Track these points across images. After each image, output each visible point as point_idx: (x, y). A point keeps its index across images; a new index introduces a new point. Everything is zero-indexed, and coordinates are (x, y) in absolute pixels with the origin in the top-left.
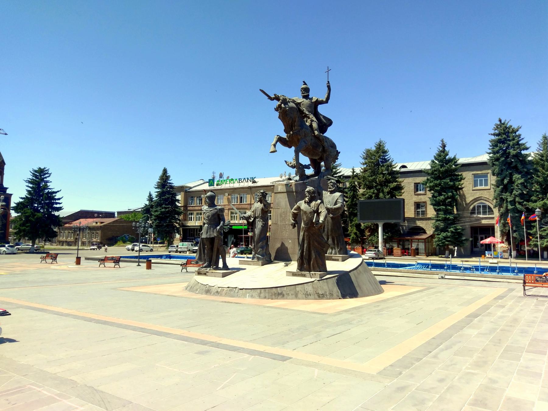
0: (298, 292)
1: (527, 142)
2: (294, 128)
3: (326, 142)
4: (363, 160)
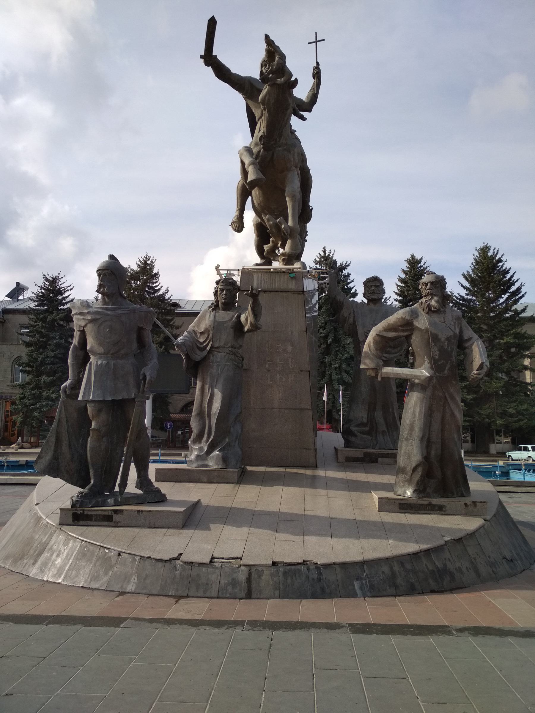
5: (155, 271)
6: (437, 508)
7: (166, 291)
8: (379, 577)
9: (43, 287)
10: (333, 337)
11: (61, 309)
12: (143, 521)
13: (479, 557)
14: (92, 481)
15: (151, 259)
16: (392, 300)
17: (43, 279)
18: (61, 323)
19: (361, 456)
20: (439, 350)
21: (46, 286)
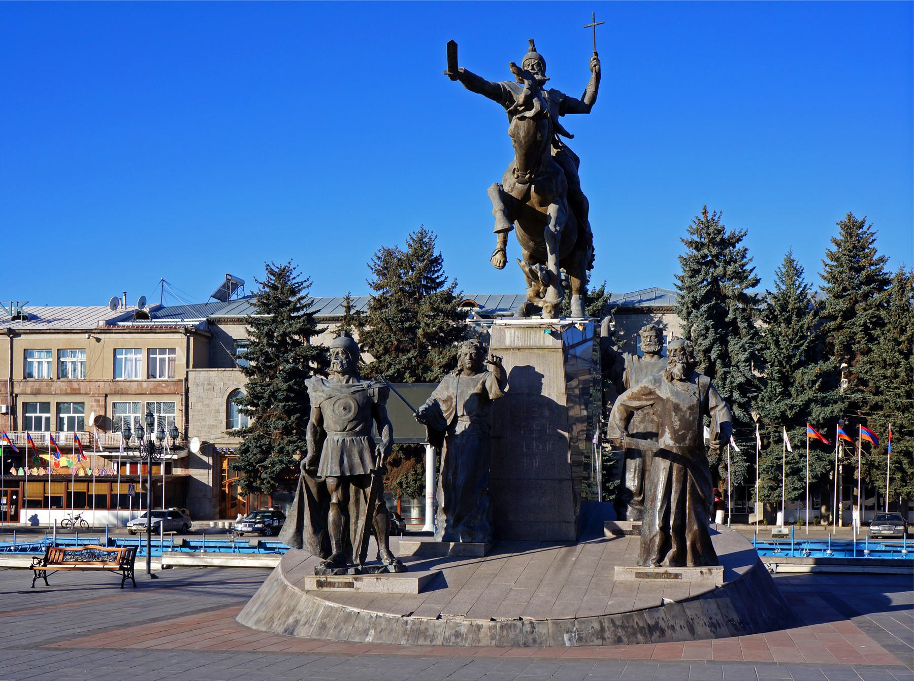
0: (692, 619)
1: (754, 268)
5: (436, 254)
6: (672, 576)
7: (454, 285)
9: (267, 283)
10: (720, 350)
11: (295, 317)
12: (382, 587)
15: (429, 235)
16: (815, 288)
17: (267, 272)
18: (296, 337)
19: (629, 529)
20: (680, 420)
21: (271, 281)
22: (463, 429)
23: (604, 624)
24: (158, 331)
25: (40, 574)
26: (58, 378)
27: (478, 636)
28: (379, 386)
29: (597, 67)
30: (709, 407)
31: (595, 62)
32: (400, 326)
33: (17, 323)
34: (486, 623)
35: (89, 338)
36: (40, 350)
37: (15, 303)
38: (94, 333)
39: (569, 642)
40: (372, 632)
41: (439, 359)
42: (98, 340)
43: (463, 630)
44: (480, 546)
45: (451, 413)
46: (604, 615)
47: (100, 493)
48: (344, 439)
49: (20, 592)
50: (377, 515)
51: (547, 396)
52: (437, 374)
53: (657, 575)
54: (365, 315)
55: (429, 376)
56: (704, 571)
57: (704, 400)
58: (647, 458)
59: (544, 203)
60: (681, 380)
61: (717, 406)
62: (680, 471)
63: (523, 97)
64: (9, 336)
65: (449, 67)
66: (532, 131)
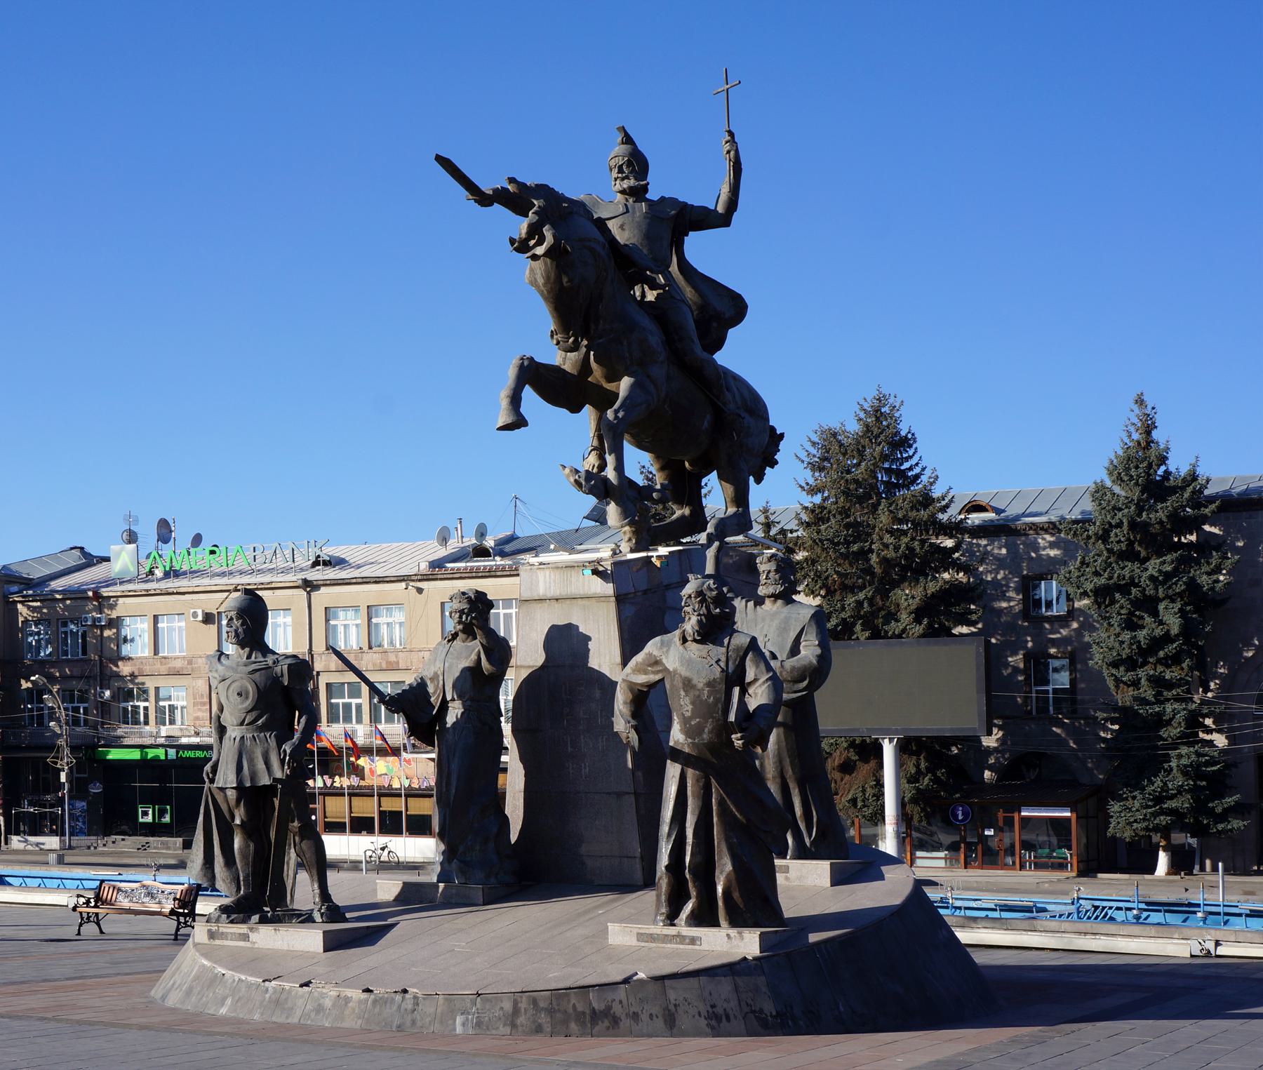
0: (675, 1005)
2: (593, 327)
3: (728, 390)
4: (809, 473)
7: (932, 480)
8: (493, 1013)
13: (689, 1004)
14: (242, 892)
20: (693, 703)
22: (455, 720)
23: (519, 1005)
24: (499, 573)
25: (89, 918)
26: (370, 648)
27: (343, 1013)
28: (289, 663)
29: (732, 153)
30: (746, 682)
31: (727, 147)
32: (842, 550)
33: (318, 570)
34: (356, 994)
35: (406, 589)
36: (345, 608)
37: (312, 542)
38: (413, 581)
39: (462, 1028)
40: (229, 1001)
41: (906, 600)
42: (420, 591)
43: (328, 1003)
44: (477, 890)
45: (439, 696)
46: (522, 992)
47: (393, 809)
48: (243, 737)
49: (41, 940)
50: (301, 842)
51: (596, 668)
52: (904, 625)
53: (666, 939)
54: (795, 534)
55: (894, 627)
56: (732, 935)
57: (734, 671)
58: (766, 761)
59: (614, 377)
60: (695, 641)
61: (756, 680)
62: (698, 781)
63: (526, 226)
64: (305, 590)
65: (466, 189)
66: (553, 274)
